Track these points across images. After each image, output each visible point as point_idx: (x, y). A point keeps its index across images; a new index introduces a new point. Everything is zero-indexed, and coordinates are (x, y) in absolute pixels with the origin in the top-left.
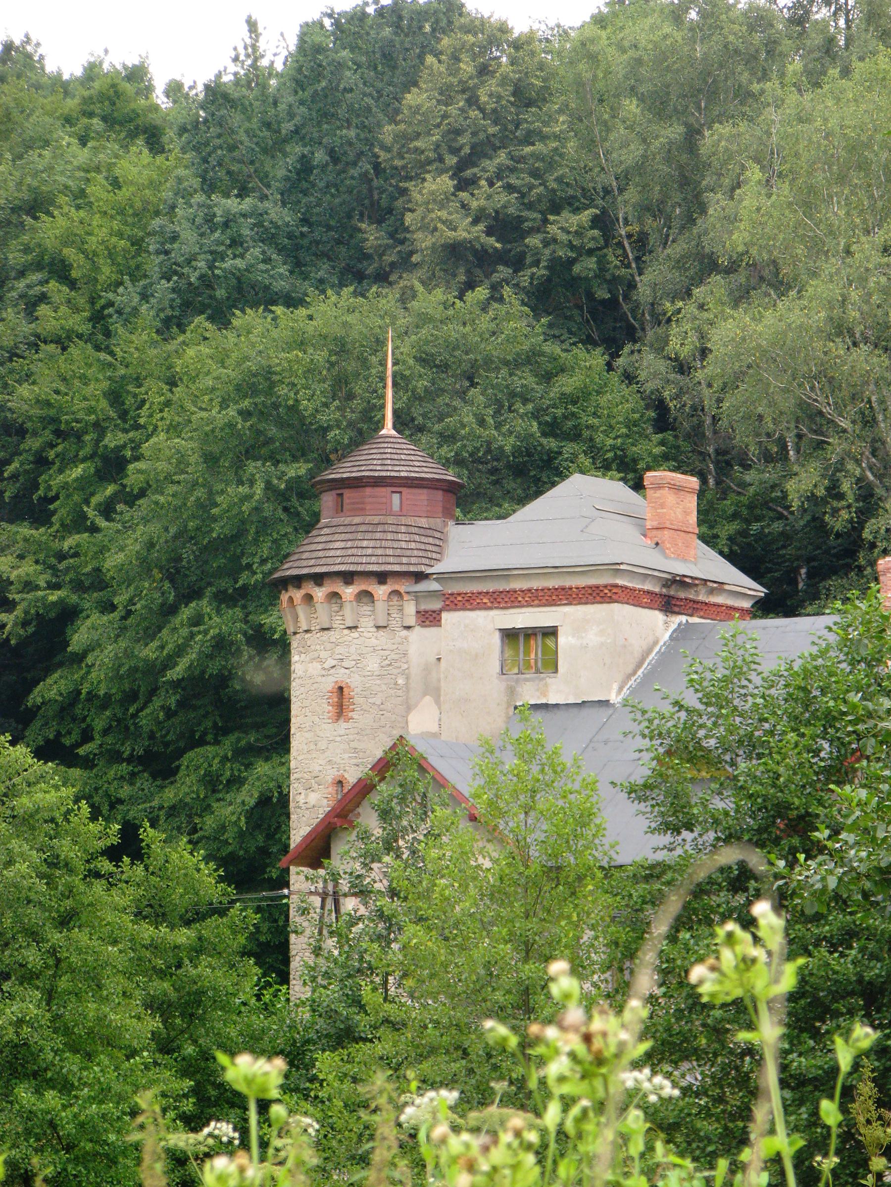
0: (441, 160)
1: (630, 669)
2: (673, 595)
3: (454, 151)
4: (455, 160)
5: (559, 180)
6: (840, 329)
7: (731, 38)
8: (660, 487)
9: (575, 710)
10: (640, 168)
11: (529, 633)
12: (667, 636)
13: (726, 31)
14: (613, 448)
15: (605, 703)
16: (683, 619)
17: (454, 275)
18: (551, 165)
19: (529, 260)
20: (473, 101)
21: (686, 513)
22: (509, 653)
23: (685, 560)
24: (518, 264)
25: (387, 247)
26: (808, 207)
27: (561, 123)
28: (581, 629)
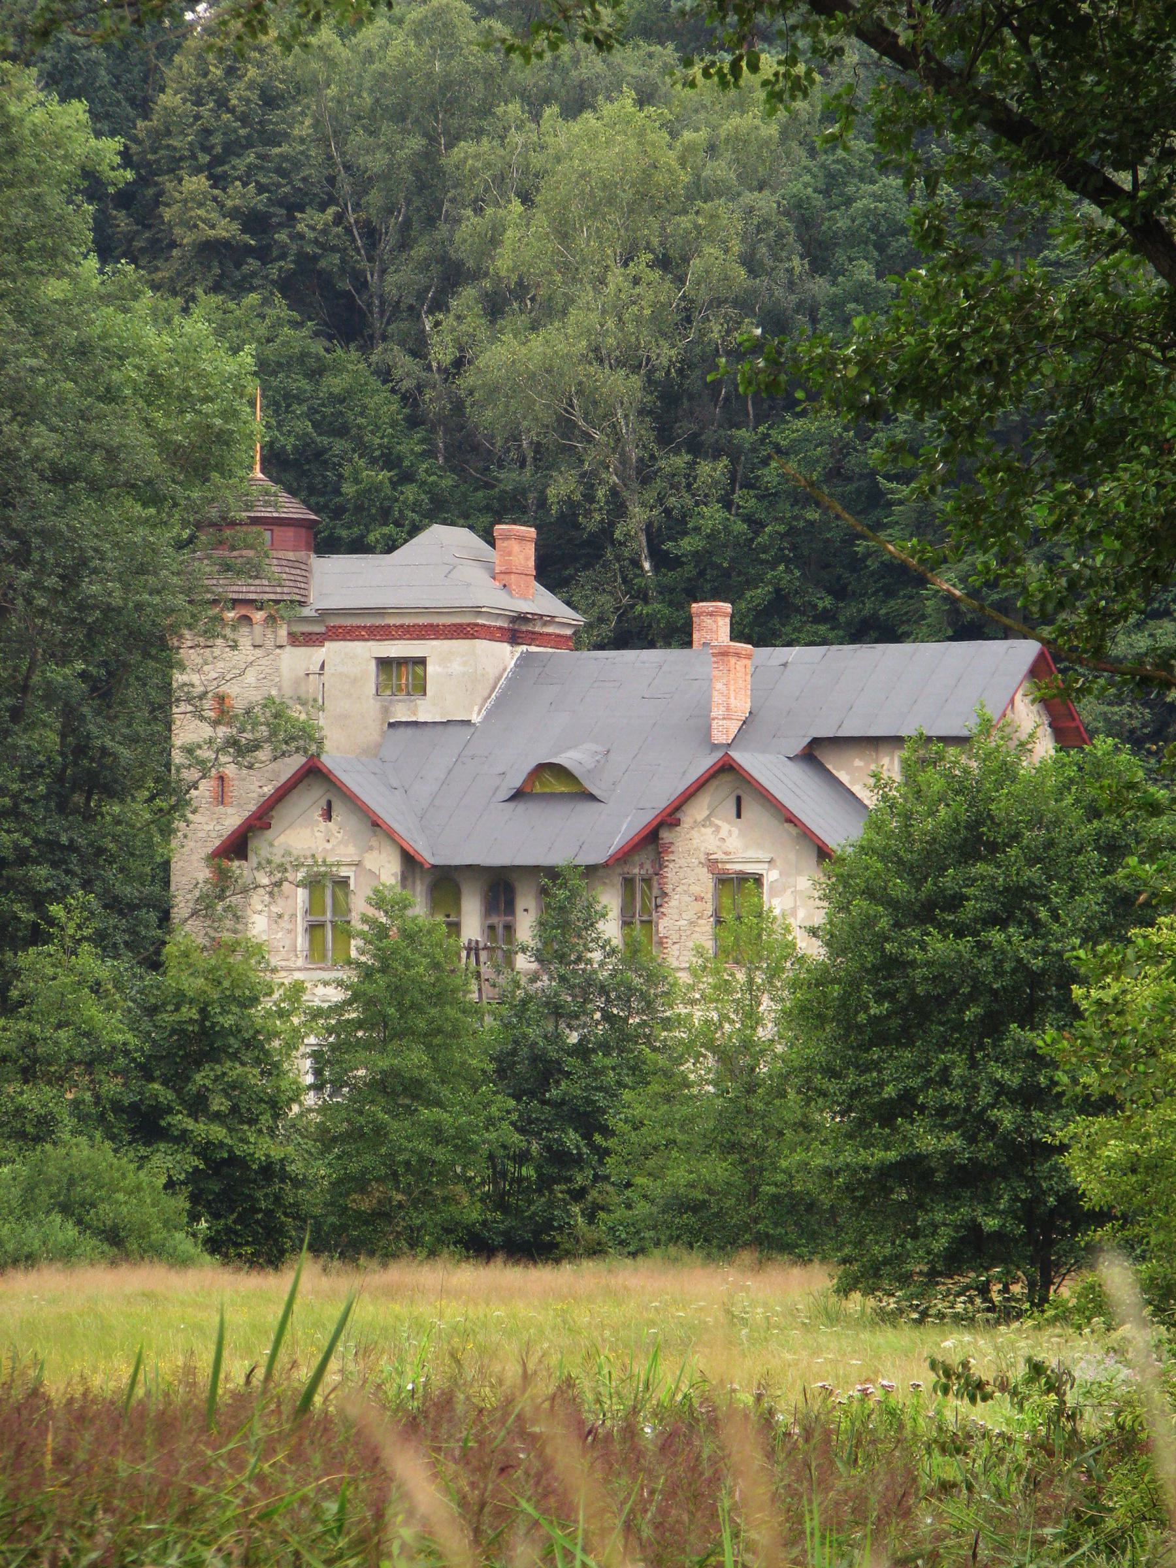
0: (194, 157)
1: (486, 694)
2: (517, 630)
3: (206, 149)
4: (208, 158)
5: (304, 179)
6: (597, 354)
7: (471, 59)
8: (507, 538)
9: (441, 728)
10: (385, 176)
11: (402, 662)
12: (512, 664)
13: (465, 52)
14: (380, 445)
15: (468, 723)
16: (524, 648)
17: (210, 268)
18: (297, 165)
19: (275, 253)
20: (223, 103)
21: (527, 559)
22: (382, 677)
23: (525, 599)
24: (263, 254)
25: (137, 232)
26: (564, 237)
27: (304, 128)
28: (445, 660)
